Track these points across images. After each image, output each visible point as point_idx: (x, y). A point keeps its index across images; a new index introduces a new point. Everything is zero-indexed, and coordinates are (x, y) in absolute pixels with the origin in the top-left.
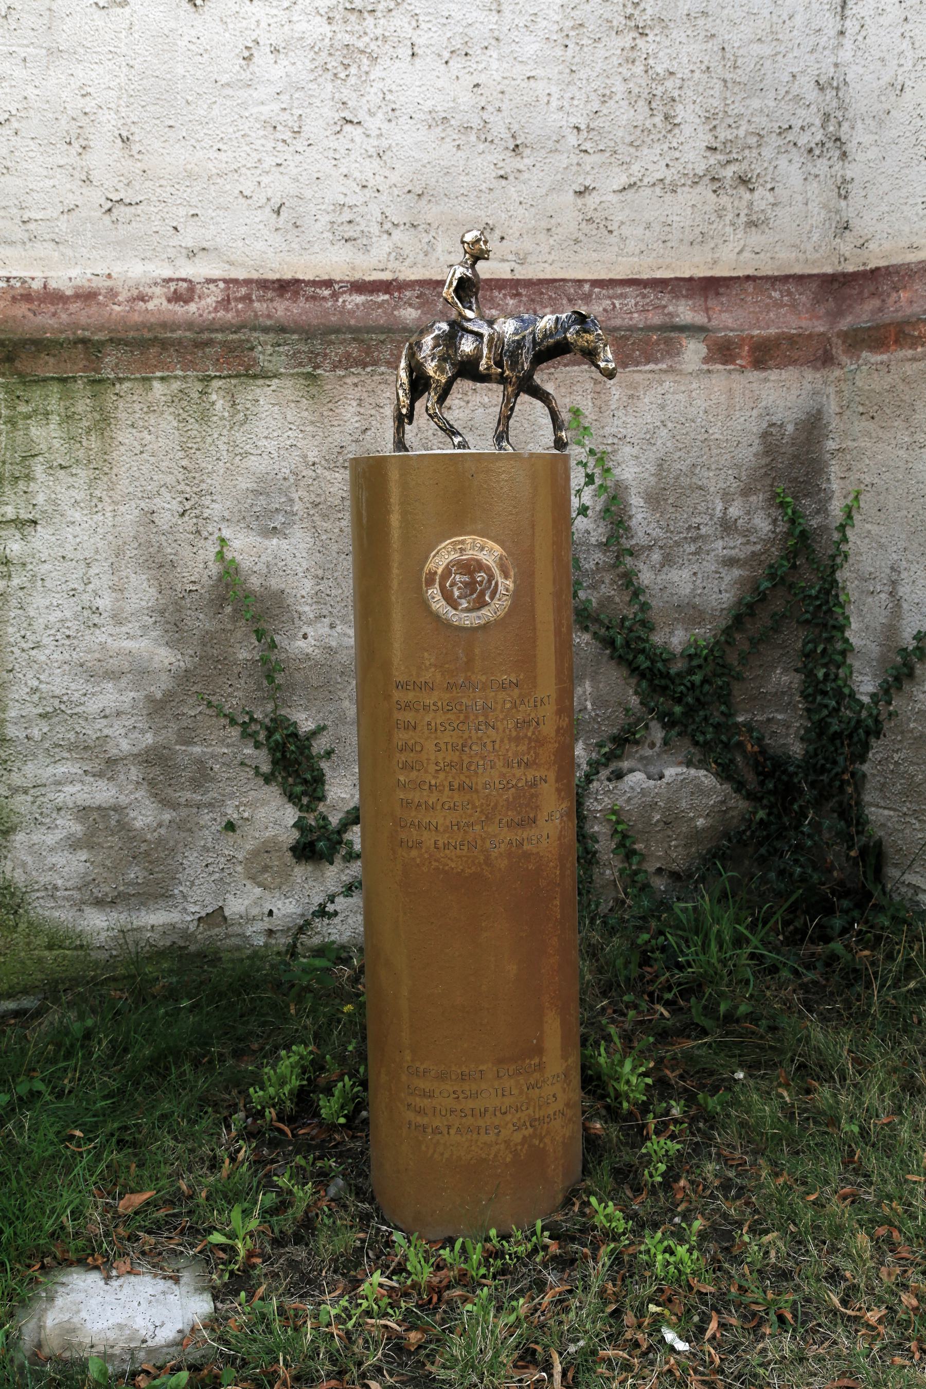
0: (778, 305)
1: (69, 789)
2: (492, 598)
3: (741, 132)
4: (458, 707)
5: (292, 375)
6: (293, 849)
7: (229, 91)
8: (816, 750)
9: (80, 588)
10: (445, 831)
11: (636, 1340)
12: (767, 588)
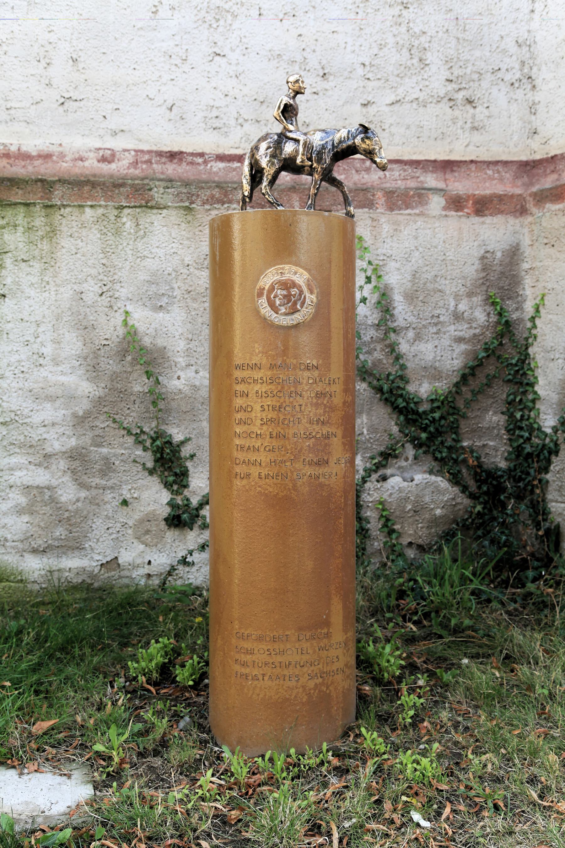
0: (491, 178)
1: (18, 473)
2: (302, 307)
3: (468, 71)
5: (176, 207)
6: (166, 520)
7: (142, 33)
8: (515, 466)
9: (32, 340)
11: (393, 819)
12: (483, 357)
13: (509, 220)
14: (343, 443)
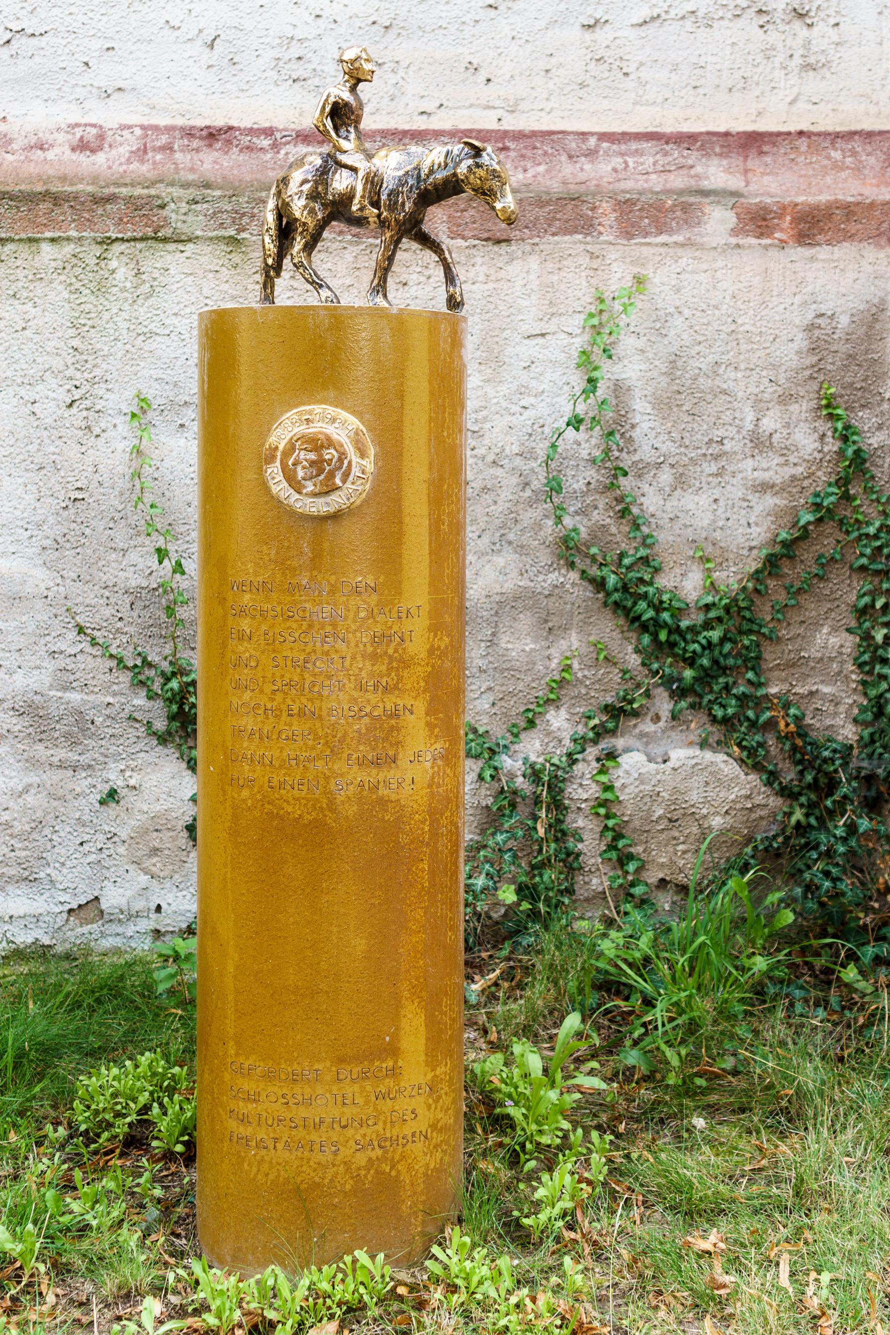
0: (838, 167)
2: (344, 481)
4: (301, 613)
5: (211, 239)
8: (872, 735)
10: (281, 766)
12: (809, 523)
13: (865, 253)
14: (428, 724)
